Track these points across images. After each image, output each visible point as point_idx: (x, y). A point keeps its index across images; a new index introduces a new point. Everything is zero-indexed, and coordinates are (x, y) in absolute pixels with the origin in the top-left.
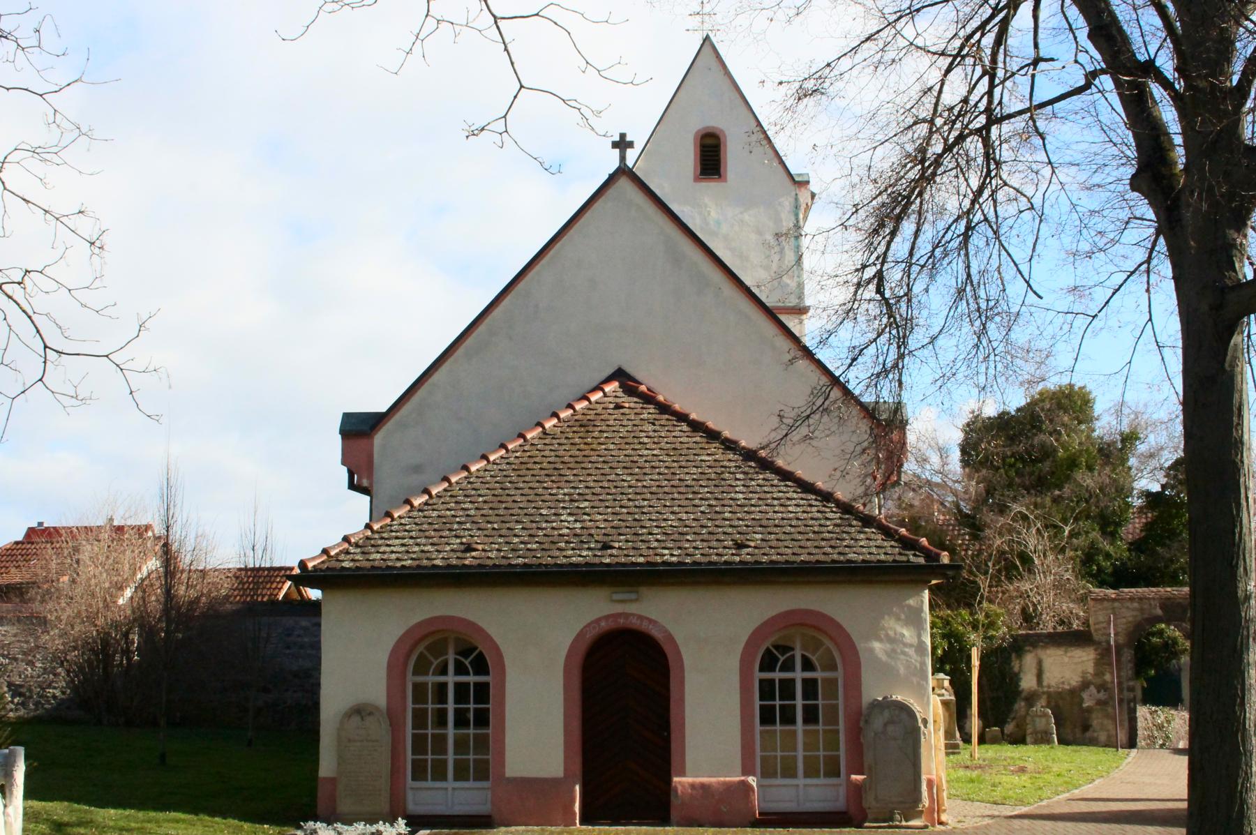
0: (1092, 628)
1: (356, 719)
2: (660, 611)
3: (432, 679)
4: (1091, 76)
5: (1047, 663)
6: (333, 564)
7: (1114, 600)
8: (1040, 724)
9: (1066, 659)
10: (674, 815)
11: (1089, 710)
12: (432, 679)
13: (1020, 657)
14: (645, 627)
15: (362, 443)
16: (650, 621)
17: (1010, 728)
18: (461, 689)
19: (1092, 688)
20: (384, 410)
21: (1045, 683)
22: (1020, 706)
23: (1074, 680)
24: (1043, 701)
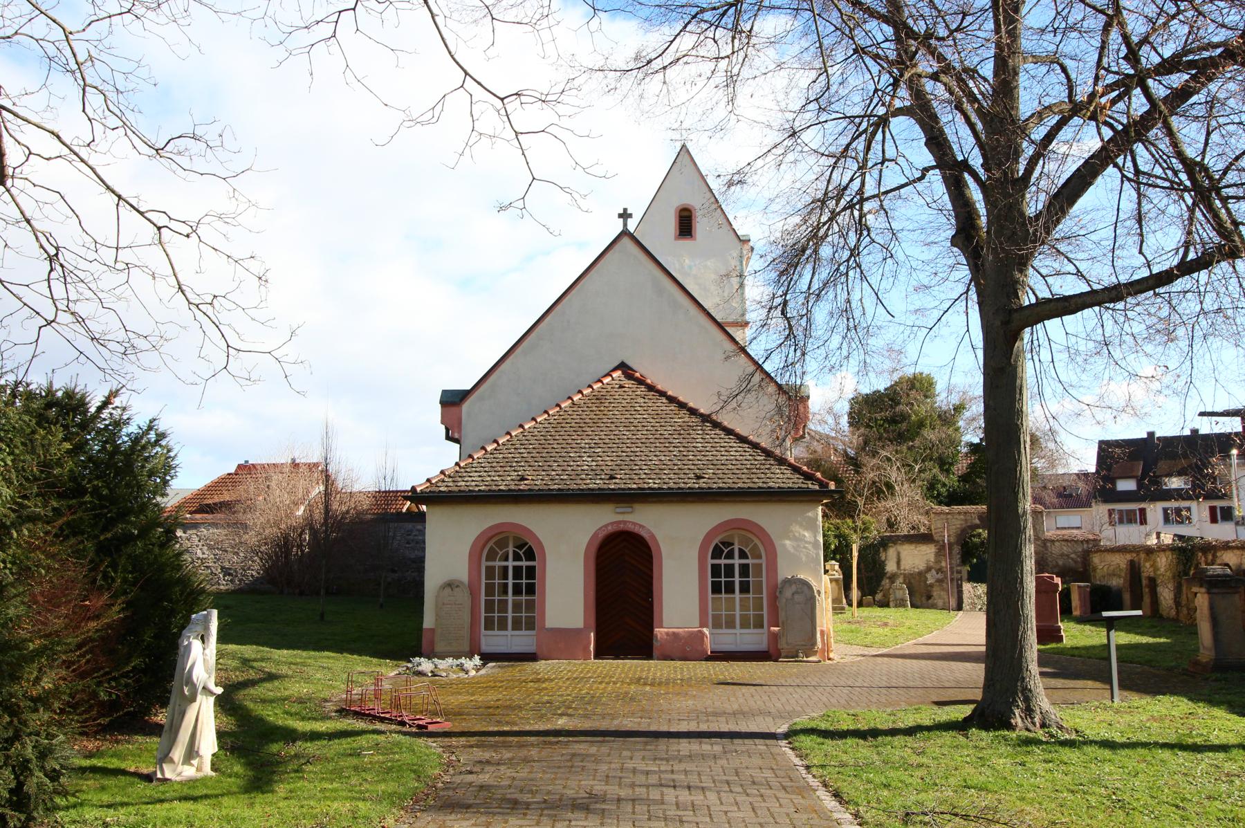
1: (448, 590)
2: (648, 520)
3: (498, 564)
6: (434, 489)
8: (899, 594)
10: (656, 653)
12: (498, 564)
13: (885, 550)
14: (637, 530)
15: (453, 410)
16: (641, 526)
17: (879, 597)
18: (517, 572)
20: (469, 388)
22: (886, 582)
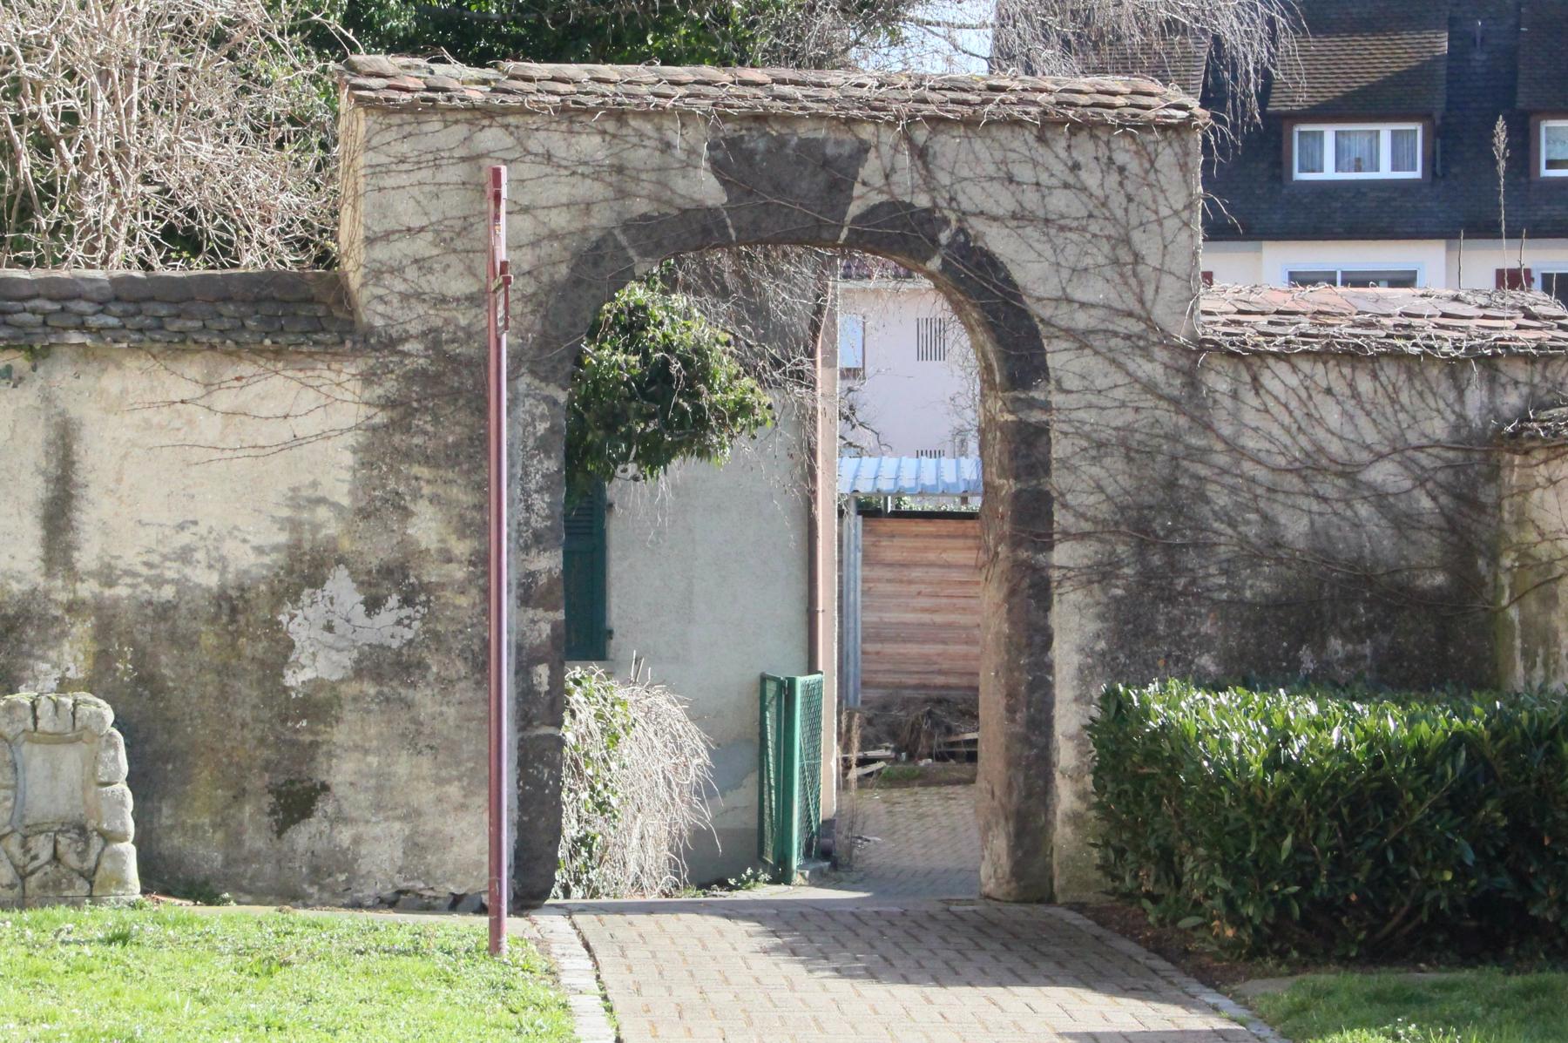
0: (353, 271)
4: (984, 25)
5: (98, 455)
7: (485, 113)
9: (209, 428)
11: (318, 706)
19: (342, 589)
21: (86, 558)
23: (248, 545)
24: (73, 654)
